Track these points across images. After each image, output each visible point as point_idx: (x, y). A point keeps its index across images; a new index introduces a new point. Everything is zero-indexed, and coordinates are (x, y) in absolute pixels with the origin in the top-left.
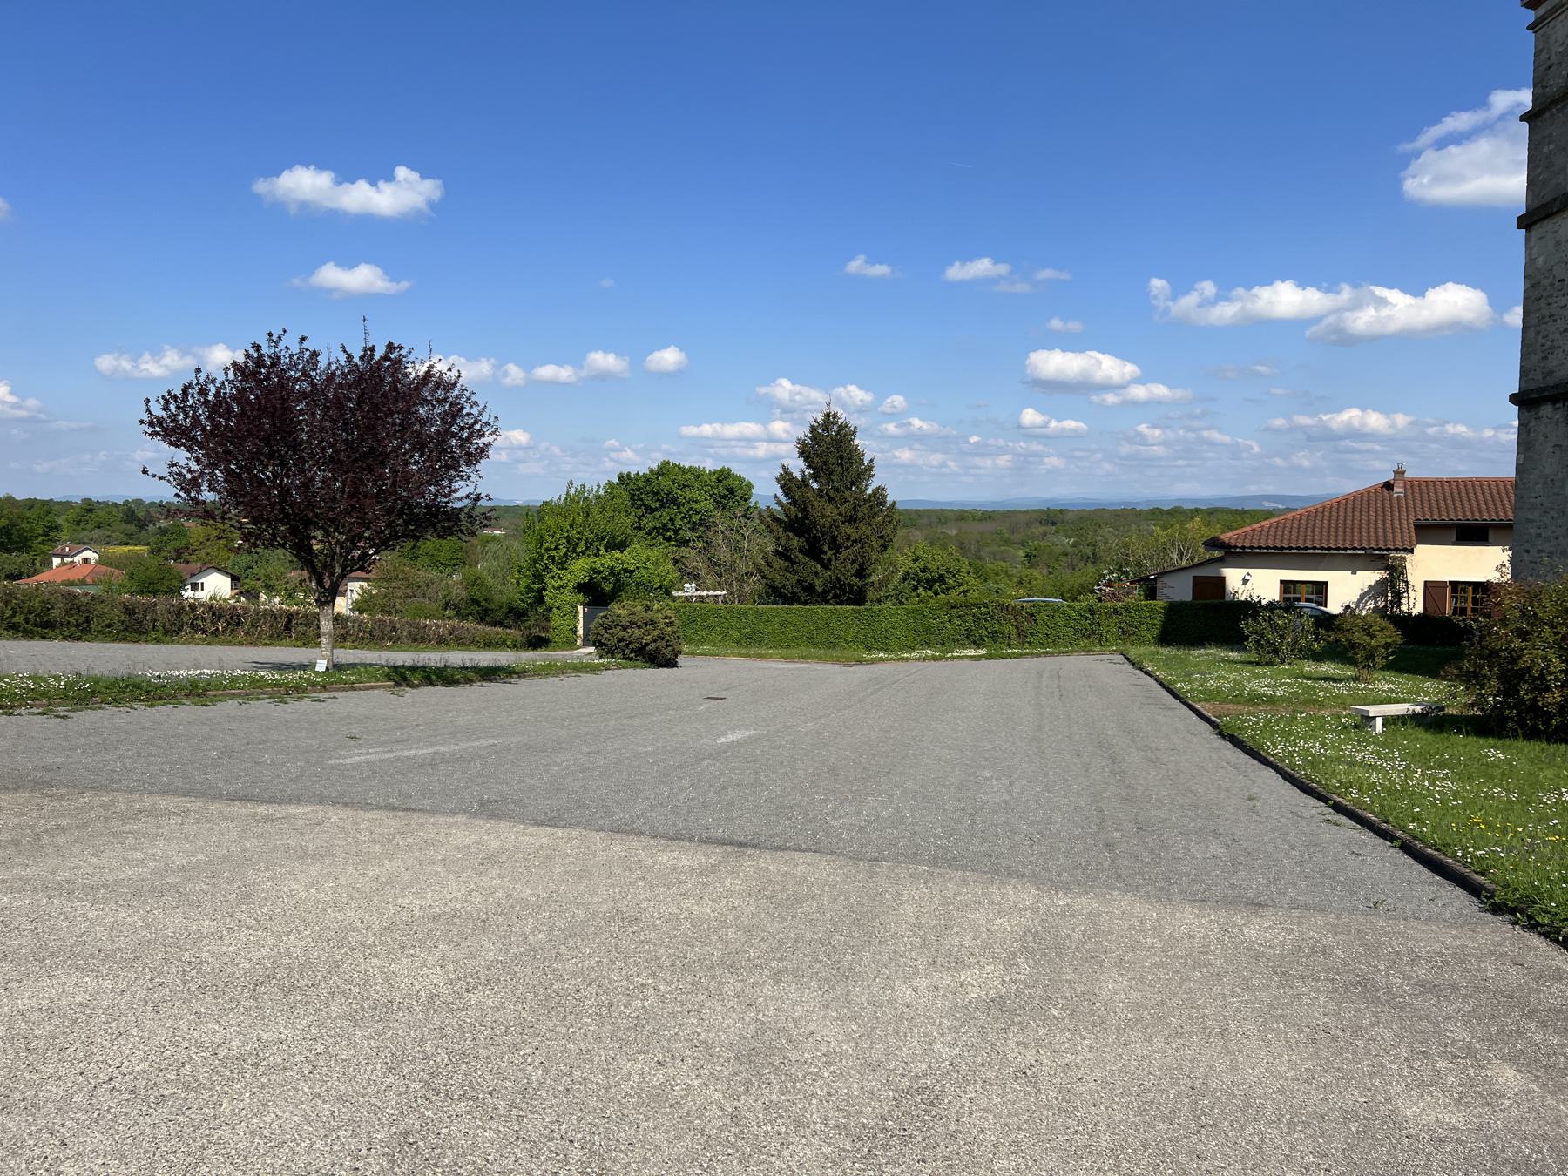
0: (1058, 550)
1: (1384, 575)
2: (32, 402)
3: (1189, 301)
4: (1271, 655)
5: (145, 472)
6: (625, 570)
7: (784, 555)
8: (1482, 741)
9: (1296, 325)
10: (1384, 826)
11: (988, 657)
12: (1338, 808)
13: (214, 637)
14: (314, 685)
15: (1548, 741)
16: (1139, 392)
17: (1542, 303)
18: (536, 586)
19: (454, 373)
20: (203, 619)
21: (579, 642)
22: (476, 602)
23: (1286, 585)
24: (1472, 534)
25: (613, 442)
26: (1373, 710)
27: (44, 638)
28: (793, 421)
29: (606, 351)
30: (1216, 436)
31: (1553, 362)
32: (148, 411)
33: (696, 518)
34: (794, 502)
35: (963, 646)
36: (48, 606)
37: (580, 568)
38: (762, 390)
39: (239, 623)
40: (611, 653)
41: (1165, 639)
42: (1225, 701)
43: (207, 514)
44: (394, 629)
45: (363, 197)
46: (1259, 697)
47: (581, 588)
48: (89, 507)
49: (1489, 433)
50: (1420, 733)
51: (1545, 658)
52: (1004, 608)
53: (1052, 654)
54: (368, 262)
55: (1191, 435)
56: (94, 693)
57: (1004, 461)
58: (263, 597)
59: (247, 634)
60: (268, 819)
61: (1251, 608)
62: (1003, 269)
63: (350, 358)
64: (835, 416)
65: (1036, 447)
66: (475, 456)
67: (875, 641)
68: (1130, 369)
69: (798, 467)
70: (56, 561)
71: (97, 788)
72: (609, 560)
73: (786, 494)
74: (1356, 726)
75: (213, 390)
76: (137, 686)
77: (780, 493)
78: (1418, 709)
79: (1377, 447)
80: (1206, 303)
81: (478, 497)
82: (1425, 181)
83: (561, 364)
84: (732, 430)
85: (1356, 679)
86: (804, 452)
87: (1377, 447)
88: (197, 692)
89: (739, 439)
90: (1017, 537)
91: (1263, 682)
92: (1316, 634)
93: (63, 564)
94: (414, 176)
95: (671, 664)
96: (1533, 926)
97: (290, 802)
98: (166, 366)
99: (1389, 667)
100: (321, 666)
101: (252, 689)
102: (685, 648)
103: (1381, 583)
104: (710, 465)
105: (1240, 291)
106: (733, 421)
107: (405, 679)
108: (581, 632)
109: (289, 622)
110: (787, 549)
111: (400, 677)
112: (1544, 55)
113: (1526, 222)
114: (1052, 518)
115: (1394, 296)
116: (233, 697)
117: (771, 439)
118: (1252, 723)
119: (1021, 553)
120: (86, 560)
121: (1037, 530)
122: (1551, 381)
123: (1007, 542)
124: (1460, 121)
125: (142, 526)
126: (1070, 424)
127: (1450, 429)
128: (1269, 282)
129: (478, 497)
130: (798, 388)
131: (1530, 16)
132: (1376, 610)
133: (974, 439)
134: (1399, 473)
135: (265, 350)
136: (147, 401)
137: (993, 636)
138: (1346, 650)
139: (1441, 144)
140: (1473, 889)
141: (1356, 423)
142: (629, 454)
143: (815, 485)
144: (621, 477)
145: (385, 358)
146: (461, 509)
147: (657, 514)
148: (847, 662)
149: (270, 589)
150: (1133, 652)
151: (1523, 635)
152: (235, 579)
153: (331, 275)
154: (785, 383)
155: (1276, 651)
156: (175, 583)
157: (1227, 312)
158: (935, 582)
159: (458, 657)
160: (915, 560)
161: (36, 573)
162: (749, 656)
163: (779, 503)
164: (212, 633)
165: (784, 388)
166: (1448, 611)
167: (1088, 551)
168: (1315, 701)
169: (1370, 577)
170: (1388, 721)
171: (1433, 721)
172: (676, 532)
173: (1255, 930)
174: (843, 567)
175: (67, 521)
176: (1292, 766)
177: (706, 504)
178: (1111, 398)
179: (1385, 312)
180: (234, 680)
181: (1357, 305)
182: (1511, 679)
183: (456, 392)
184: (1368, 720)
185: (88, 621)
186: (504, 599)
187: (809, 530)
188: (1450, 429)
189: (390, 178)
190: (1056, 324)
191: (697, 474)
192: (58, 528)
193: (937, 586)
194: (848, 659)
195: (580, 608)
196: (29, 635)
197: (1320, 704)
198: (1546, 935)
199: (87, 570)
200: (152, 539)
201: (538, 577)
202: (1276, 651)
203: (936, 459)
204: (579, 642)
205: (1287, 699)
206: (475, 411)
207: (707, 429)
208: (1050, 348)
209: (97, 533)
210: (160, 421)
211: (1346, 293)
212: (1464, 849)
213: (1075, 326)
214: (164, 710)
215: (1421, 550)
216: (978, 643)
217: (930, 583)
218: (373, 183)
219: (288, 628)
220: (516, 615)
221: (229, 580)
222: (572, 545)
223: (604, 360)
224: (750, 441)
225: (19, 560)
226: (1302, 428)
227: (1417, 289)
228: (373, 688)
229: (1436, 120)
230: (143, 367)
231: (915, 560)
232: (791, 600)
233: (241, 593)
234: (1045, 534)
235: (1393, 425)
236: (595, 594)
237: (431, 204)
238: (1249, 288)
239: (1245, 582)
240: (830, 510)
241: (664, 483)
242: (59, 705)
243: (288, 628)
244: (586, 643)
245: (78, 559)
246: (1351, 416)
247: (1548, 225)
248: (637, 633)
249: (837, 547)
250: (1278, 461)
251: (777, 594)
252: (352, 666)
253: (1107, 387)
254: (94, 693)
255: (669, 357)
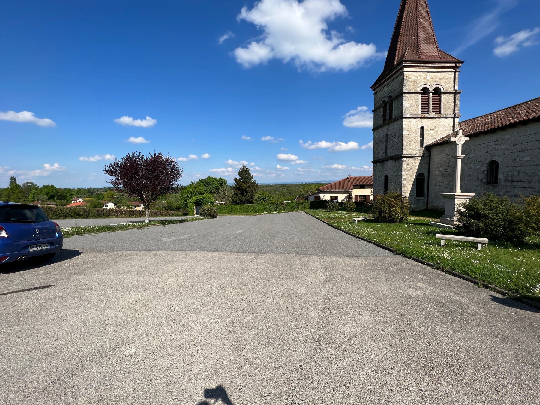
0: (285, 192)
1: (348, 194)
2: (64, 167)
3: (307, 145)
4: (332, 210)
5: (106, 182)
6: (204, 199)
7: (236, 194)
8: (375, 224)
9: (326, 149)
10: (369, 240)
11: (278, 213)
12: (358, 237)
13: (117, 216)
14: (146, 225)
15: (386, 223)
16: (298, 162)
17: (377, 144)
18: (185, 203)
19: (174, 159)
20: (114, 213)
21: (195, 214)
22: (169, 207)
23: (331, 197)
24: (362, 187)
25: (195, 173)
26: (356, 219)
27: (79, 218)
28: (232, 168)
29: (193, 154)
30: (312, 170)
31: (379, 155)
32: (105, 168)
33: (216, 188)
34: (238, 184)
35: (273, 211)
36: (79, 211)
37: (194, 199)
38: (226, 162)
39: (122, 213)
40: (204, 216)
41: (311, 208)
42: (327, 219)
43: (121, 190)
44: (156, 213)
45: (139, 123)
46: (333, 218)
47: (195, 203)
48: (79, 190)
49: (359, 168)
50: (364, 223)
51: (386, 208)
52: (281, 203)
53: (290, 212)
54: (141, 136)
55: (308, 170)
56: (99, 230)
57: (274, 175)
58: (122, 208)
59: (124, 215)
60: (156, 254)
61: (326, 202)
62: (272, 138)
63: (152, 155)
64: (245, 166)
65: (280, 172)
66: (178, 176)
67: (256, 211)
68: (297, 157)
69: (238, 177)
70: (73, 202)
71: (113, 250)
72: (200, 197)
73: (236, 182)
74: (353, 222)
75: (120, 163)
76: (108, 228)
77: (235, 183)
78: (363, 219)
79: (341, 171)
80: (310, 145)
81: (178, 185)
82: (347, 122)
83: (184, 157)
84: (220, 170)
85: (348, 214)
86: (239, 174)
87: (341, 171)
88: (122, 228)
89: (221, 172)
90: (277, 190)
91: (332, 215)
92: (339, 206)
93: (74, 202)
94: (150, 119)
95: (216, 217)
96: (406, 257)
97: (158, 251)
98: (96, 159)
99: (355, 211)
100: (147, 221)
101: (133, 227)
102: (219, 214)
103: (348, 196)
104: (218, 177)
105: (316, 143)
106: (220, 168)
107: (164, 223)
108: (195, 212)
109: (133, 212)
110: (237, 193)
111: (163, 223)
112: (376, 99)
113: (373, 130)
114: (283, 186)
115: (342, 144)
116: (129, 229)
117: (228, 172)
118: (335, 222)
119: (278, 193)
120: (80, 201)
121: (281, 188)
122: (379, 159)
123: (275, 191)
124: (353, 112)
125: (92, 193)
126: (286, 168)
127: (353, 168)
128: (321, 141)
129: (178, 185)
130: (233, 161)
131: (373, 92)
132: (347, 201)
133: (268, 171)
134: (349, 176)
135: (131, 155)
136: (105, 166)
137: (279, 209)
138: (347, 208)
139: (349, 116)
140: (391, 251)
141: (337, 167)
142: (198, 175)
143: (242, 180)
144: (200, 180)
145: (158, 156)
146: (175, 187)
147: (208, 187)
148: (251, 215)
149: (124, 206)
150: (306, 211)
151: (382, 204)
152: (115, 204)
153: (133, 139)
154: (230, 160)
155: (332, 209)
156: (102, 205)
157: (313, 147)
158: (264, 199)
159: (169, 218)
160: (260, 195)
161: (68, 204)
162: (231, 215)
163: (235, 184)
164: (117, 216)
165: (230, 161)
166: (359, 201)
167: (291, 192)
168: (343, 218)
169: (346, 195)
170: (358, 221)
171: (366, 221)
172: (212, 191)
173: (361, 261)
174: (248, 196)
175: (75, 193)
176: (346, 230)
177: (217, 185)
178: (293, 163)
179: (341, 147)
180: (129, 225)
181: (336, 145)
182: (380, 212)
183: (174, 163)
184: (355, 221)
185: (88, 214)
186: (175, 206)
187: (241, 189)
188: (353, 168)
189: (145, 119)
190: (283, 149)
191: (215, 179)
192: (73, 195)
193: (265, 200)
194: (251, 215)
195: (195, 207)
196: (75, 218)
197: (344, 218)
198: (408, 258)
199: (80, 204)
200: (95, 196)
201: (186, 201)
202: (332, 209)
203: (261, 175)
204: (195, 214)
205: (338, 218)
206: (178, 167)
207: (215, 170)
208: (282, 153)
209: (82, 195)
210: (108, 170)
211: (334, 143)
212: (387, 243)
213: (286, 149)
214: (115, 233)
215: (354, 189)
216: (276, 211)
217: (263, 199)
218: (142, 120)
219: (133, 214)
220: (178, 209)
221: (114, 204)
222: (193, 194)
223: (193, 156)
224: (224, 172)
225: (64, 202)
226: (327, 168)
227: (346, 142)
228: (158, 225)
229: (348, 112)
230: (90, 159)
231: (260, 195)
232: (238, 203)
233: (117, 207)
234: (282, 189)
235: (343, 167)
236: (198, 204)
237: (155, 124)
238: (317, 142)
239: (324, 197)
240: (245, 185)
241: (209, 181)
242: (92, 233)
243: (133, 214)
244: (197, 214)
245: (78, 201)
246: (336, 166)
247: (378, 130)
248: (209, 212)
249: (247, 193)
250: (323, 174)
251: (235, 202)
252: (153, 221)
253: (292, 161)
254: (99, 230)
255: (206, 156)
